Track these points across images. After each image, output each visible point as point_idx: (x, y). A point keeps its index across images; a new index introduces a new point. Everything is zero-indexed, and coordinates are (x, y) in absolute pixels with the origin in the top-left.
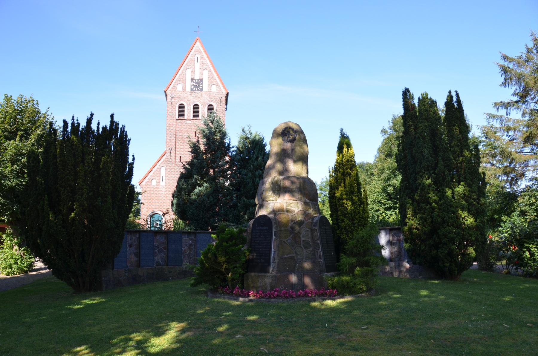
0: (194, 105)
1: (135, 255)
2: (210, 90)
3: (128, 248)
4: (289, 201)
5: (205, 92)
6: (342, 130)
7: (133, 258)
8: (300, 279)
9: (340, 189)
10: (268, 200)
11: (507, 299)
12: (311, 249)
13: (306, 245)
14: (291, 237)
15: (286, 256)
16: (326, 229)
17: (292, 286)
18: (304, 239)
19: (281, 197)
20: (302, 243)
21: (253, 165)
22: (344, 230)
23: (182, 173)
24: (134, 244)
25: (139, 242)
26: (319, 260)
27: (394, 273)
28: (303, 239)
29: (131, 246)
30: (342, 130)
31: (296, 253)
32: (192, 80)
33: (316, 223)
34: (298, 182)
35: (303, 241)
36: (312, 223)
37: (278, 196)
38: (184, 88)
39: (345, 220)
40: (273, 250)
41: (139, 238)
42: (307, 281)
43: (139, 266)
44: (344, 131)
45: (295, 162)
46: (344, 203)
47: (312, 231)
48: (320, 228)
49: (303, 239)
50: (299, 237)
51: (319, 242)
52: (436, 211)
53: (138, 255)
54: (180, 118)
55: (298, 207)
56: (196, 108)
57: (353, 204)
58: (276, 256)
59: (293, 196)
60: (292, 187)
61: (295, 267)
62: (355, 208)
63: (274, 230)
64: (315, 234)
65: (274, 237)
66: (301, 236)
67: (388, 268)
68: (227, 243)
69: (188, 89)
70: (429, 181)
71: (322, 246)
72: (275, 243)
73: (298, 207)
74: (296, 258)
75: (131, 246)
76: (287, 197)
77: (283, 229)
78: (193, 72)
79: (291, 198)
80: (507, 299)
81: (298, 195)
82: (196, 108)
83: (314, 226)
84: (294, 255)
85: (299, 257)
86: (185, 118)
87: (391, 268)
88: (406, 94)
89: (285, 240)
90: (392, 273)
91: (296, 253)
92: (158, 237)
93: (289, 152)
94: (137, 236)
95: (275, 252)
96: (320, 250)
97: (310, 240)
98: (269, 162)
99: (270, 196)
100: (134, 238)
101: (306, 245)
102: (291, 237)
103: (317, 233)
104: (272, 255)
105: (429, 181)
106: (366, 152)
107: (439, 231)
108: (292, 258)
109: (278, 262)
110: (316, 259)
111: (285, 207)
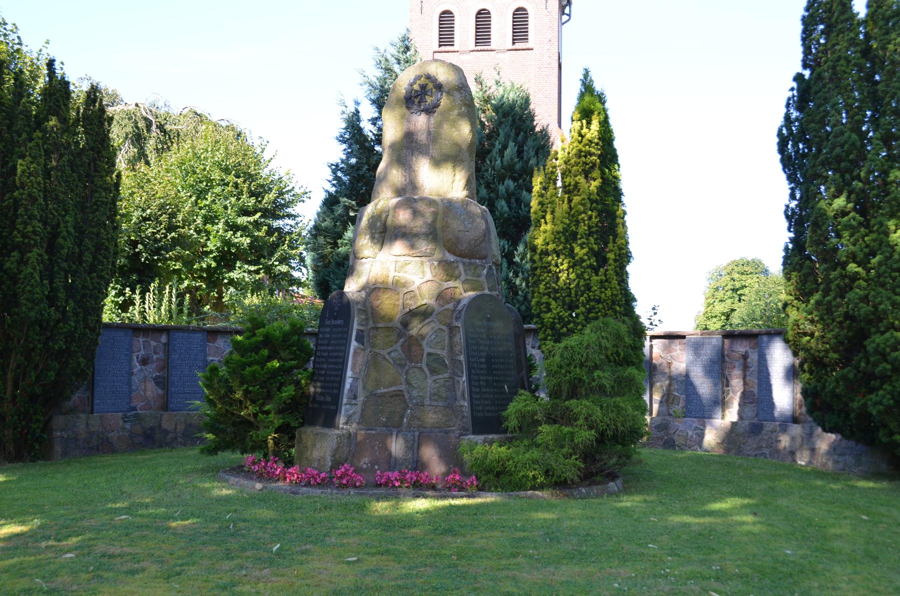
0: (479, 13)
1: (157, 384)
3: (137, 366)
4: (402, 259)
6: (586, 74)
7: (152, 390)
8: (414, 447)
9: (543, 228)
10: (361, 256)
11: (864, 517)
12: (446, 375)
13: (436, 365)
14: (399, 344)
15: (383, 390)
17: (391, 462)
18: (431, 351)
19: (386, 249)
21: (493, 168)
22: (549, 331)
23: (330, 194)
24: (155, 357)
25: (168, 353)
27: (798, 455)
28: (427, 350)
29: (144, 362)
30: (586, 74)
31: (408, 383)
33: (460, 312)
34: (428, 211)
35: (429, 354)
36: (454, 311)
37: (378, 246)
39: (553, 304)
40: (349, 373)
41: (167, 345)
42: (430, 453)
43: (165, 407)
44: (593, 75)
45: (437, 163)
46: (549, 263)
47: (452, 330)
49: (427, 350)
50: (420, 345)
51: (462, 358)
52: (859, 287)
53: (162, 382)
54: (443, 48)
55: (423, 272)
56: (483, 18)
57: (572, 266)
59: (412, 247)
60: (412, 225)
61: (402, 417)
62: (578, 276)
63: (356, 326)
65: (354, 344)
67: (785, 441)
68: (242, 356)
70: (840, 202)
71: (469, 370)
72: (360, 360)
73: (423, 272)
74: (407, 397)
75: (144, 362)
76: (399, 247)
77: (380, 325)
79: (406, 251)
80: (864, 517)
81: (424, 246)
82: (483, 18)
83: (457, 319)
84: (403, 387)
85: (415, 393)
86: (493, 46)
87: (793, 439)
89: (384, 353)
90: (792, 453)
91: (408, 383)
93: (422, 137)
94: (164, 339)
95: (355, 379)
96: (464, 378)
97: (444, 353)
98: (382, 165)
99: (365, 246)
100: (153, 343)
101: (436, 365)
102: (399, 344)
103: (460, 338)
104: (347, 386)
105: (840, 202)
107: (866, 343)
108: (399, 395)
109: (365, 403)
110: (456, 399)
111: (392, 275)
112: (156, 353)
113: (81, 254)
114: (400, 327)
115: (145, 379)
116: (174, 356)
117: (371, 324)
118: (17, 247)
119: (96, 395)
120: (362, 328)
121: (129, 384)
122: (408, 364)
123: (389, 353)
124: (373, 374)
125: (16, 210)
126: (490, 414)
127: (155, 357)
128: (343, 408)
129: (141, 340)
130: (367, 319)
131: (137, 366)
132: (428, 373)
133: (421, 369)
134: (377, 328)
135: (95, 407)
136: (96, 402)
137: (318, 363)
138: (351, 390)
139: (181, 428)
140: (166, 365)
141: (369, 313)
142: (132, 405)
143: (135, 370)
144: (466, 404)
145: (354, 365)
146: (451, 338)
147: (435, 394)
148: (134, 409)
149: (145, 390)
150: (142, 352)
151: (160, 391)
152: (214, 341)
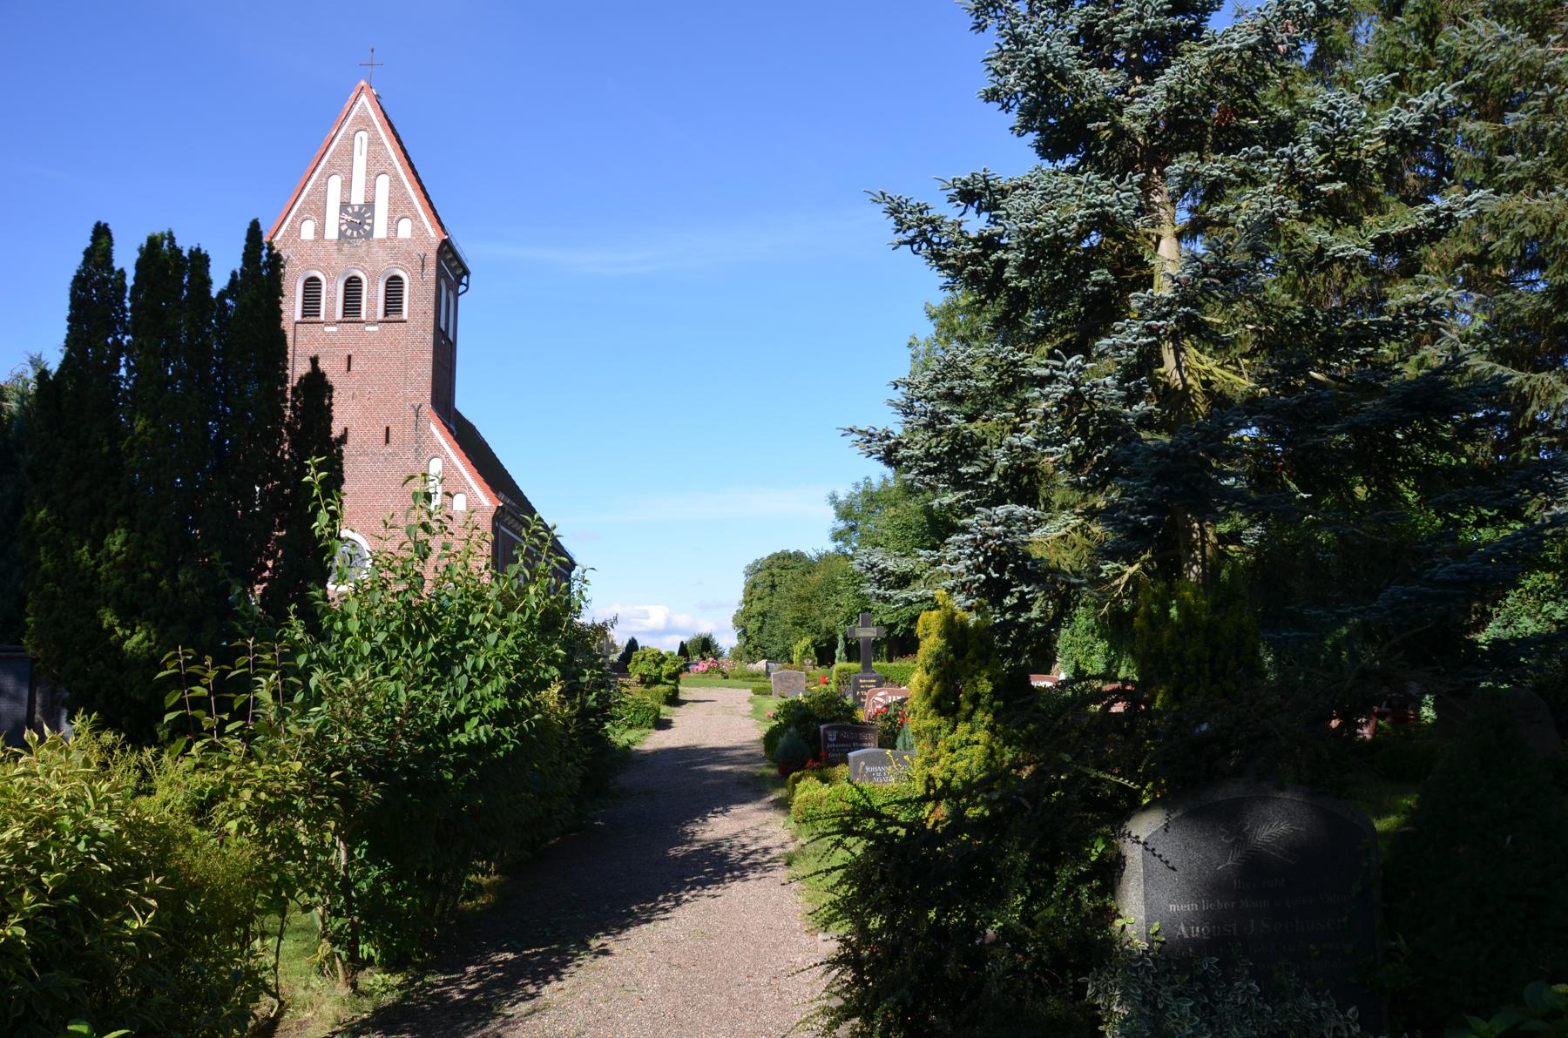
5: (380, 241)
32: (344, 206)
38: (320, 231)
69: (332, 233)
78: (347, 185)
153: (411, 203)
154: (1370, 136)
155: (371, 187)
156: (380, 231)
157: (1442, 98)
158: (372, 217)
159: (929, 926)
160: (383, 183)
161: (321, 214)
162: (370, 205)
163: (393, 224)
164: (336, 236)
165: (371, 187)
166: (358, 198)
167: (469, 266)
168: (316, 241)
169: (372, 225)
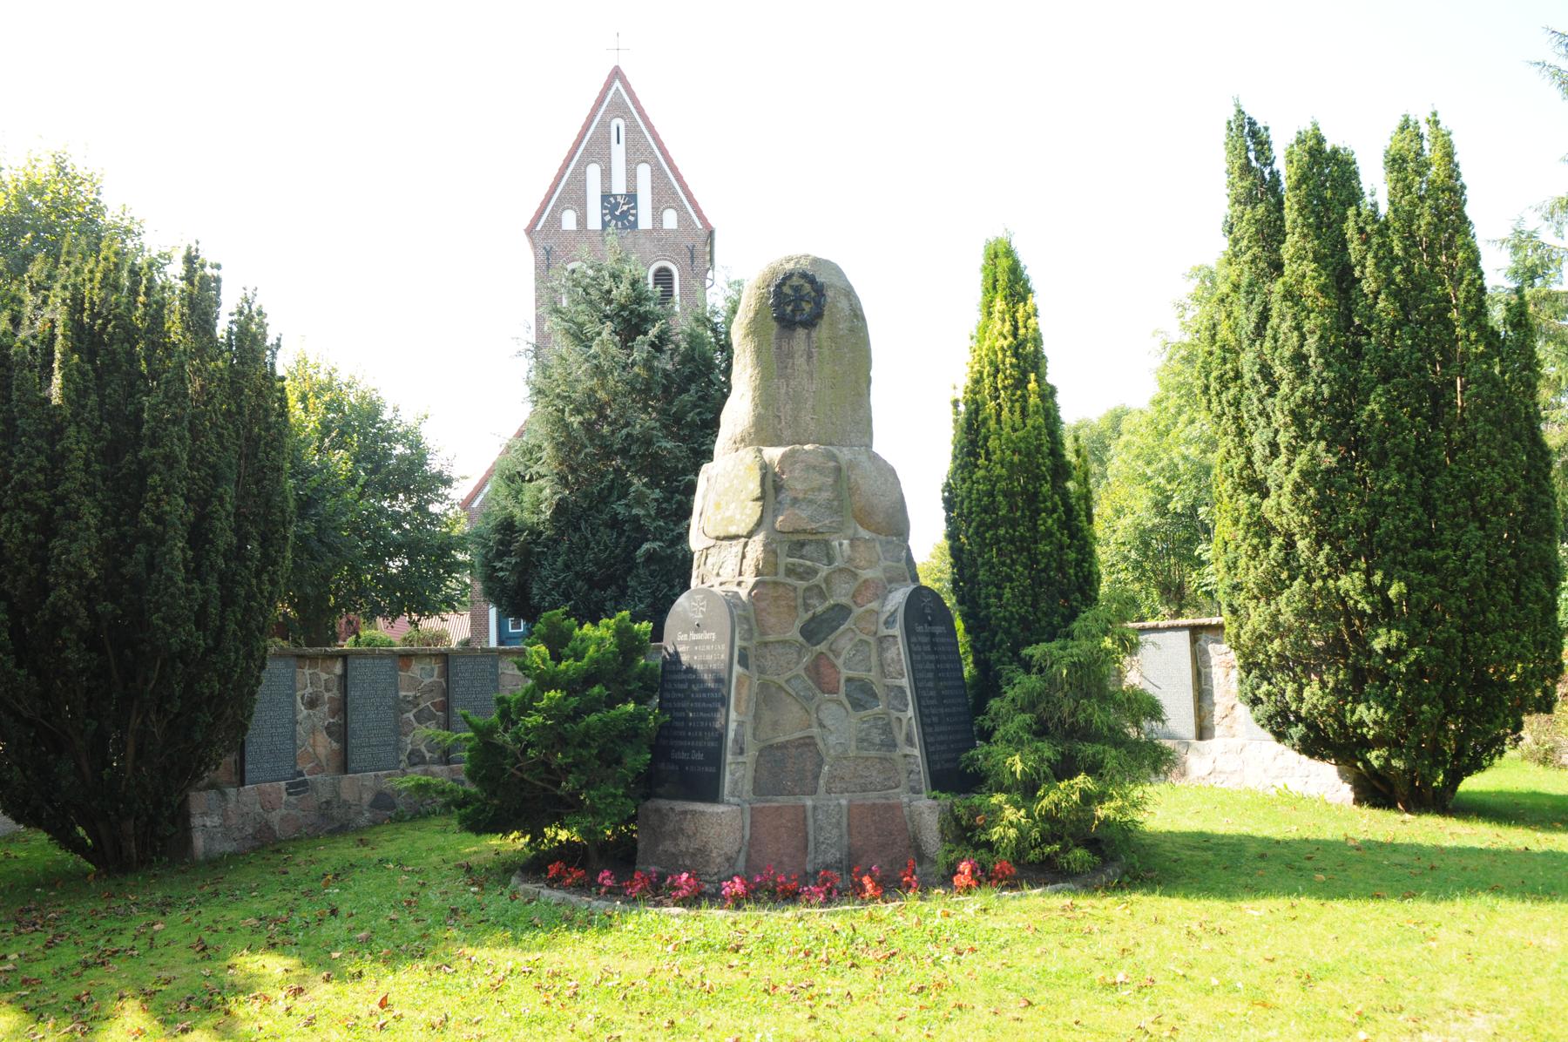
1: (330, 734)
2: (658, 225)
3: (303, 711)
5: (646, 231)
7: (324, 746)
16: (933, 635)
18: (851, 674)
20: (842, 688)
24: (326, 695)
26: (908, 750)
28: (845, 673)
30: (1010, 283)
32: (606, 197)
35: (849, 680)
38: (582, 220)
41: (344, 676)
43: (344, 767)
48: (909, 631)
51: (905, 682)
53: (341, 733)
58: (748, 737)
61: (816, 777)
64: (891, 654)
66: (839, 662)
69: (594, 222)
71: (919, 698)
72: (745, 692)
74: (821, 745)
75: (312, 703)
77: (771, 638)
78: (606, 174)
88: (1250, 137)
91: (822, 725)
92: (416, 669)
94: (338, 668)
95: (741, 724)
96: (910, 712)
100: (324, 676)
106: (1118, 372)
112: (328, 690)
113: (241, 547)
114: (801, 639)
115: (313, 730)
116: (354, 693)
117: (757, 639)
118: (147, 536)
119: (248, 758)
120: (744, 644)
121: (293, 738)
122: (819, 695)
123: (787, 681)
124: (768, 716)
125: (143, 479)
126: (947, 765)
127: (326, 695)
128: (727, 769)
129: (307, 672)
130: (750, 630)
131: (303, 711)
132: (849, 706)
133: (840, 703)
134: (766, 644)
135: (248, 776)
136: (248, 767)
137: (669, 700)
138: (736, 741)
139: (368, 797)
140: (342, 707)
141: (753, 621)
142: (298, 768)
143: (300, 717)
144: (917, 752)
145: (738, 701)
146: (880, 655)
147: (862, 740)
148: (301, 774)
149: (314, 746)
150: (309, 690)
151: (335, 745)
152: (407, 667)
153: (675, 193)
154: (1465, 642)
155: (631, 177)
156: (645, 221)
157: (27, 959)
158: (603, 215)
159: (569, 695)
160: (644, 172)
161: (581, 205)
162: (632, 197)
163: (657, 216)
164: (599, 226)
165: (631, 177)
166: (619, 187)
167: (979, 260)
168: (579, 231)
169: (635, 216)
